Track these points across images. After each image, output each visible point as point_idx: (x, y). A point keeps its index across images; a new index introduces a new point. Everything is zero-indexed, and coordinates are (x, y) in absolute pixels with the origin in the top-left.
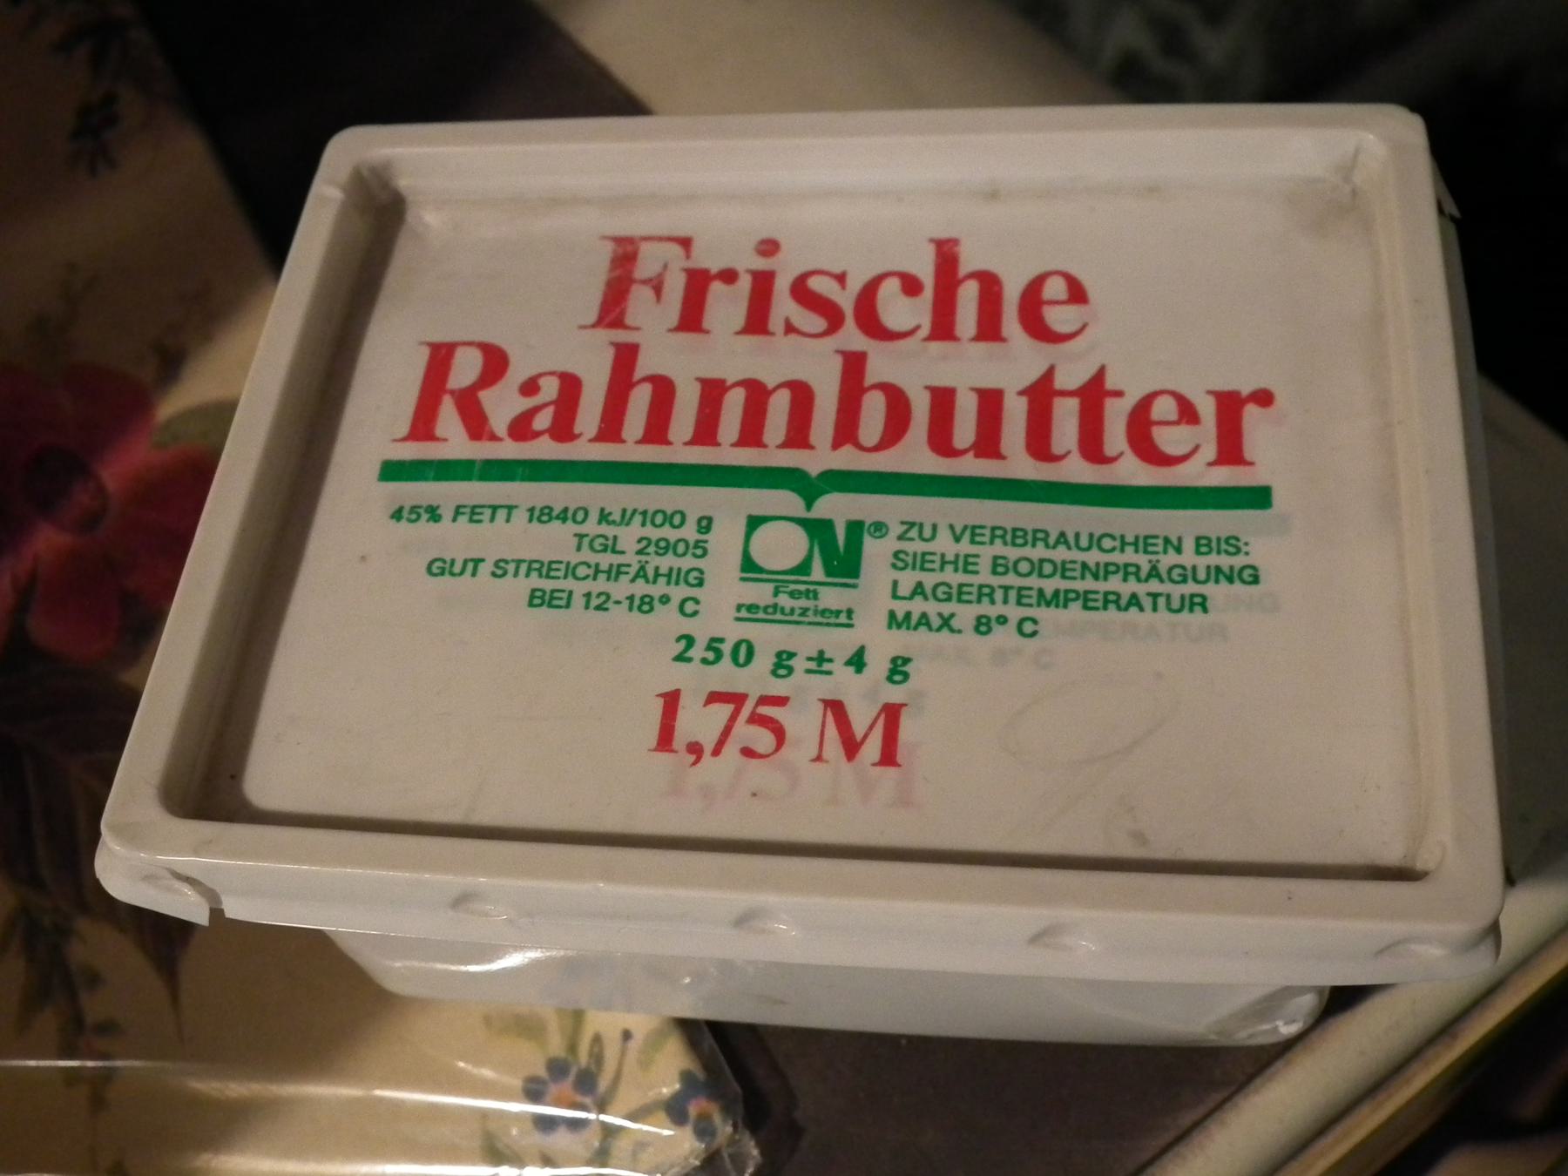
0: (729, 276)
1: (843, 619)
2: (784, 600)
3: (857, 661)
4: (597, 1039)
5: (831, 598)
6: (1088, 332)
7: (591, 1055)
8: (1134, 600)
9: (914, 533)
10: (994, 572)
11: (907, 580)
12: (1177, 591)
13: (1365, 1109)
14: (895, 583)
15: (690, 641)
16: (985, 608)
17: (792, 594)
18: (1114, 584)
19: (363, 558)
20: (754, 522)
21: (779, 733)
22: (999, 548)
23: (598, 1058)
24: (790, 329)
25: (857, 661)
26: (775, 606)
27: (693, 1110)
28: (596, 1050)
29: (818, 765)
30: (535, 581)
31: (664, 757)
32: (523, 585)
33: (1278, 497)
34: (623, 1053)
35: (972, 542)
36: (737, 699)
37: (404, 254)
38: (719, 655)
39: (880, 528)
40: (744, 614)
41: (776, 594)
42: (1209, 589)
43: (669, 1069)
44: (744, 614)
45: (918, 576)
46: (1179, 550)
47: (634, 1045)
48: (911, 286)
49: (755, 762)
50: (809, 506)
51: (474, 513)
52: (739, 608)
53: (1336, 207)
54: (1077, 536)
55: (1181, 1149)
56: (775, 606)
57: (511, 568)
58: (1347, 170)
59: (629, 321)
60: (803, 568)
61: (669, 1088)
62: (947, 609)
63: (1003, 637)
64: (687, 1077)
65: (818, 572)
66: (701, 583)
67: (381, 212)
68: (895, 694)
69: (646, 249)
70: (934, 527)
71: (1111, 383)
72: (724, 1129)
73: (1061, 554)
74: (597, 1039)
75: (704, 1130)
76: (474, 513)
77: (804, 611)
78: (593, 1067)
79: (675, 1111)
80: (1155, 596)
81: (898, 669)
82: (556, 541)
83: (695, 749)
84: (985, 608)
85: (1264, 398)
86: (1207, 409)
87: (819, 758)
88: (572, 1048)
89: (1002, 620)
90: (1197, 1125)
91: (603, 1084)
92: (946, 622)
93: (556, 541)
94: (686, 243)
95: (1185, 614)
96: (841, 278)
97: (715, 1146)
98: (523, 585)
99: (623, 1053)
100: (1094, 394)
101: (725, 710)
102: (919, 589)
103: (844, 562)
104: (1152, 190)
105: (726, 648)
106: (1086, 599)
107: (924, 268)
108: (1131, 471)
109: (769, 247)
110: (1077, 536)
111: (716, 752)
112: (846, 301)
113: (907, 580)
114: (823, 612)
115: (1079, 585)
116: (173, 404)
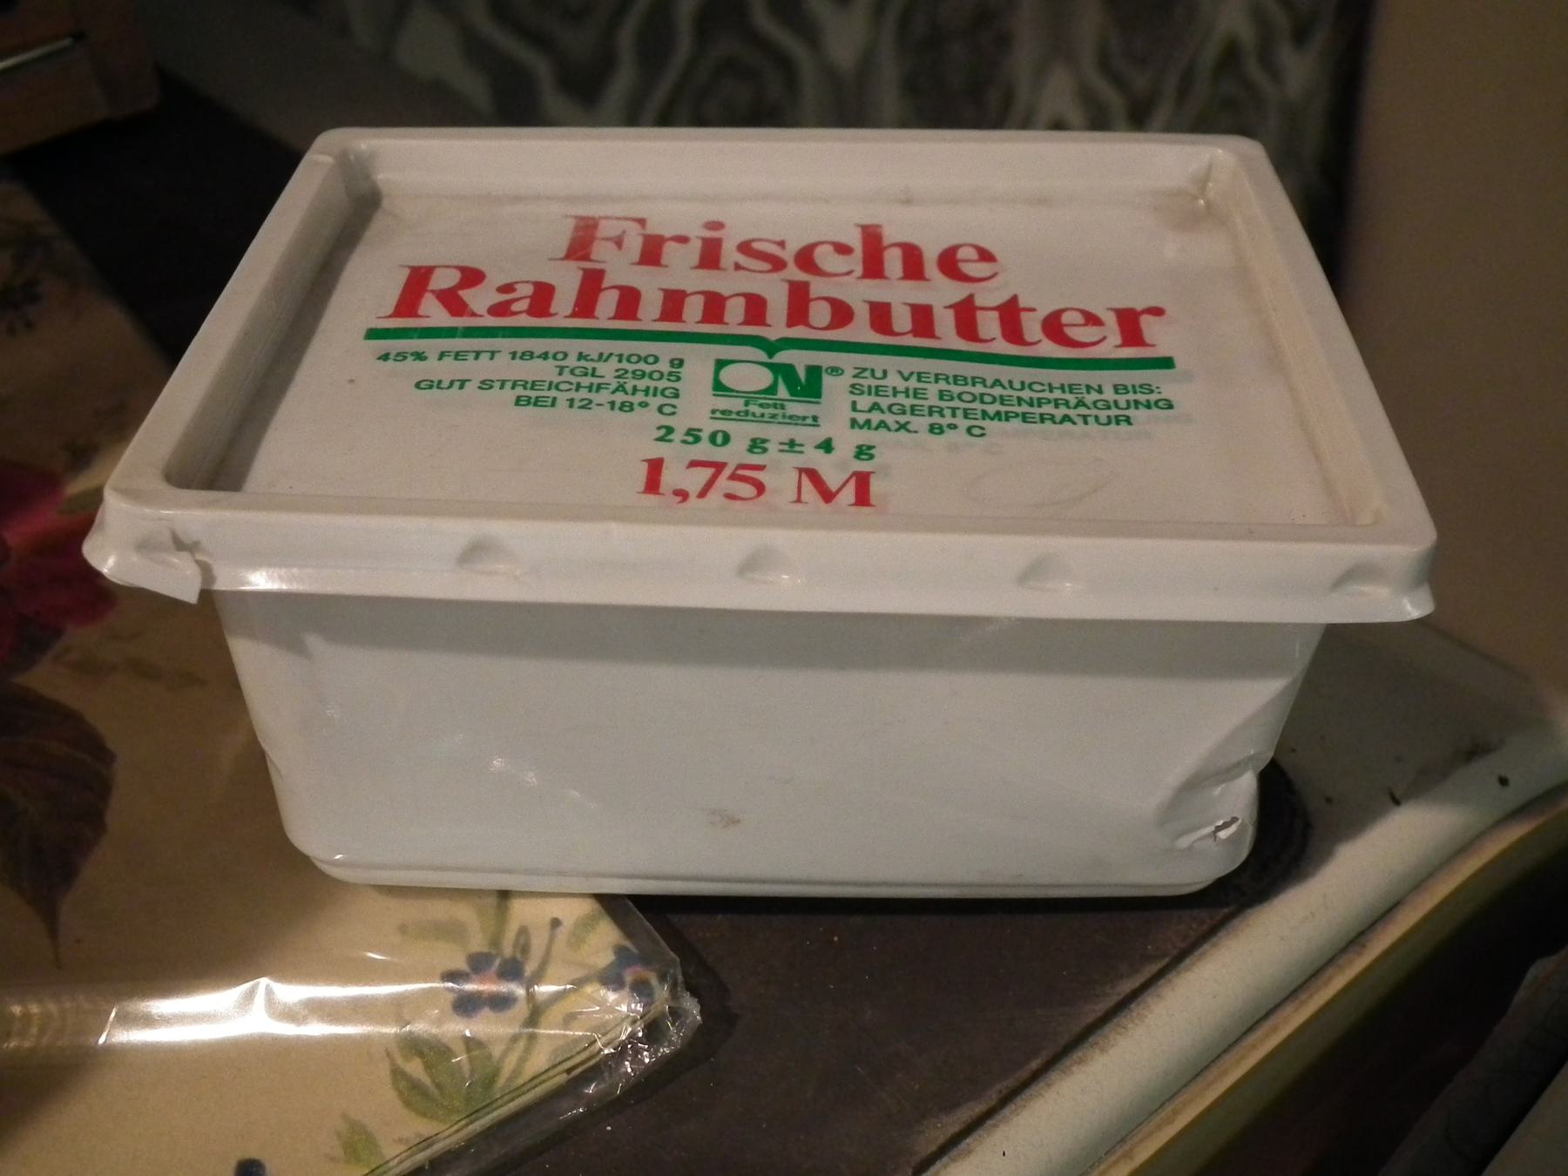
0: (683, 240)
1: (809, 421)
2: (753, 408)
3: (827, 446)
4: (523, 931)
5: (795, 408)
6: (999, 278)
7: (516, 945)
8: (1066, 418)
9: (867, 374)
10: (941, 398)
11: (864, 402)
12: (1103, 415)
13: (1289, 1009)
14: (854, 403)
15: (670, 430)
16: (936, 419)
17: (761, 405)
18: (1048, 409)
19: (351, 381)
20: (721, 364)
21: (760, 488)
22: (942, 385)
23: (525, 949)
24: (738, 267)
25: (827, 446)
26: (747, 413)
27: (629, 978)
28: (522, 941)
29: (799, 506)
30: (520, 391)
31: (652, 499)
32: (509, 394)
33: (1177, 361)
34: (552, 938)
35: (919, 380)
36: (719, 467)
37: (378, 224)
38: (697, 439)
39: (836, 371)
40: (718, 415)
41: (747, 404)
42: (1131, 412)
43: (605, 939)
44: (718, 415)
45: (873, 399)
46: (1100, 391)
47: (562, 934)
48: (842, 249)
49: (738, 503)
50: (771, 356)
51: (457, 356)
52: (713, 412)
53: (1192, 211)
54: (1010, 382)
55: (1120, 1019)
56: (747, 413)
57: (497, 385)
58: (1202, 181)
59: (593, 257)
60: (772, 389)
61: (606, 958)
62: (902, 419)
63: (959, 436)
64: (620, 951)
65: (783, 392)
66: (677, 396)
67: (358, 211)
68: (863, 466)
69: (603, 224)
70: (885, 372)
71: (1022, 303)
72: (662, 992)
73: (997, 391)
74: (523, 931)
75: (641, 989)
76: (457, 356)
77: (773, 416)
78: (519, 956)
79: (611, 979)
80: (1085, 417)
81: (863, 452)
82: (543, 370)
83: (683, 495)
84: (936, 419)
85: (1157, 312)
86: (1111, 320)
87: (799, 500)
88: (496, 942)
89: (953, 427)
90: (1135, 995)
91: (529, 969)
92: (903, 427)
93: (543, 370)
94: (642, 222)
95: (1113, 426)
96: (782, 244)
97: (653, 1012)
98: (509, 394)
99: (552, 938)
100: (1010, 314)
101: (708, 473)
102: (875, 407)
103: (809, 386)
104: (1042, 201)
105: (705, 435)
106: (1025, 418)
107: (855, 240)
108: (1049, 349)
109: (717, 225)
110: (1010, 382)
111: (703, 494)
112: (788, 255)
113: (864, 402)
114: (791, 417)
115: (1019, 410)
116: (77, 486)
